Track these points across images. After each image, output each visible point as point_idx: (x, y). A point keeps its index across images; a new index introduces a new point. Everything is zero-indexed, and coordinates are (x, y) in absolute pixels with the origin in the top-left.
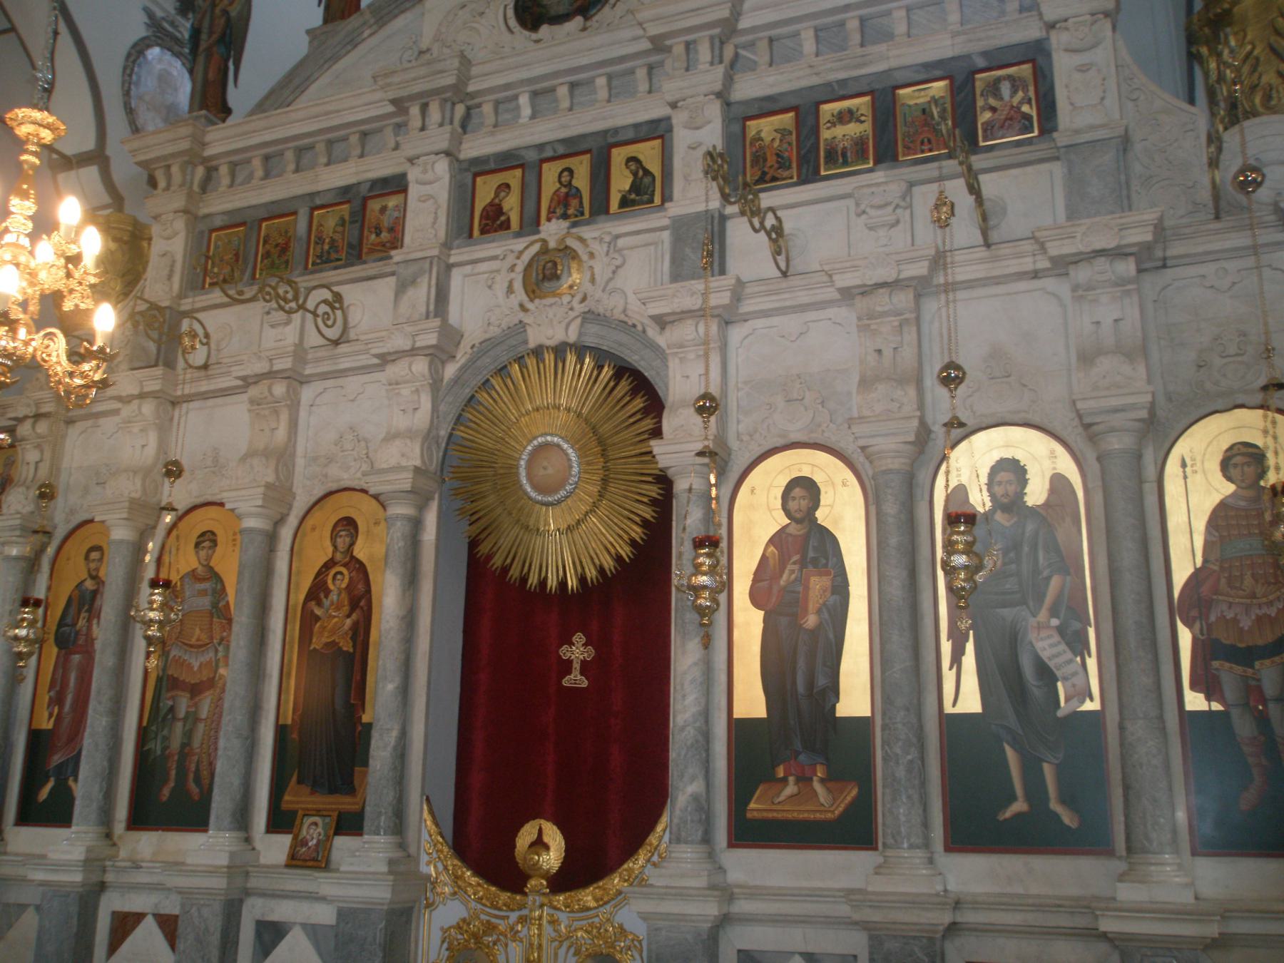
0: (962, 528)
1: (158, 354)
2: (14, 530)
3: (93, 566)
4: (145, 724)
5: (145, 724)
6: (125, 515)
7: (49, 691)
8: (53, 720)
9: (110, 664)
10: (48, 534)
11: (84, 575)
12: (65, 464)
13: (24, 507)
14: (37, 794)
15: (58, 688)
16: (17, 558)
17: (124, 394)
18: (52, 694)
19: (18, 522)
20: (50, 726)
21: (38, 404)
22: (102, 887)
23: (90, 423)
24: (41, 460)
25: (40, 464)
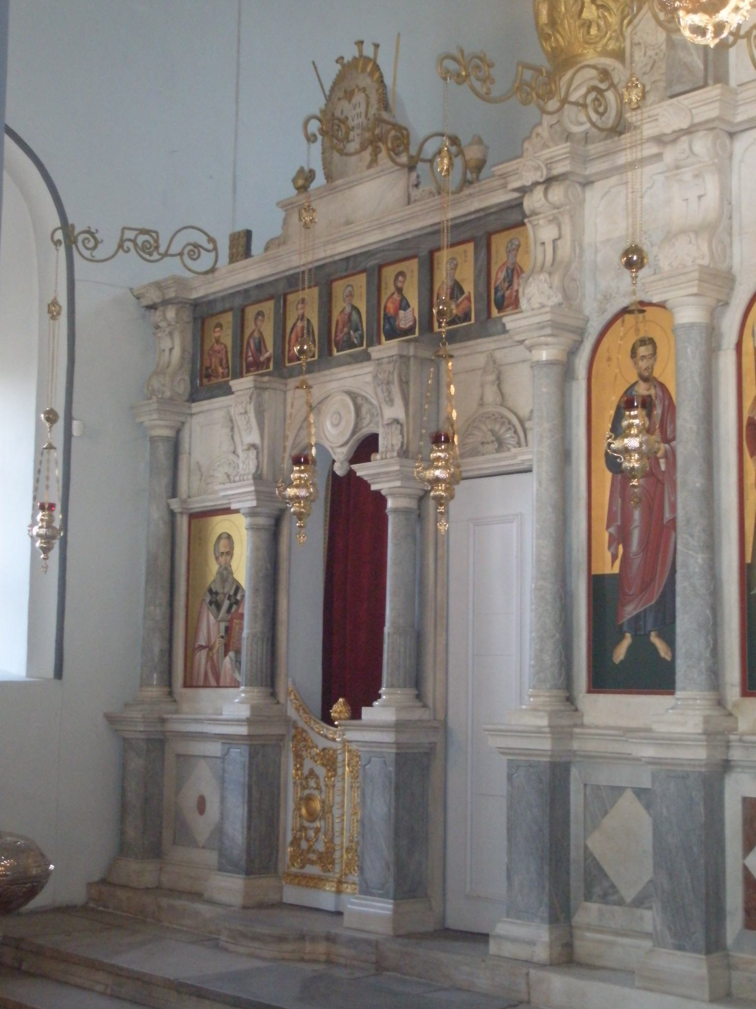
0: (443, 447)
1: (706, 69)
2: (543, 328)
3: (643, 364)
4: (748, 560)
5: (748, 560)
6: (695, 290)
7: (608, 527)
8: (618, 563)
9: (698, 485)
10: (581, 332)
11: (634, 378)
12: (587, 239)
13: (549, 298)
14: (612, 652)
15: (619, 523)
16: (550, 363)
17: (668, 131)
18: (612, 530)
19: (548, 317)
20: (616, 570)
21: (549, 165)
22: (726, 766)
23: (613, 180)
24: (560, 238)
25: (559, 242)
